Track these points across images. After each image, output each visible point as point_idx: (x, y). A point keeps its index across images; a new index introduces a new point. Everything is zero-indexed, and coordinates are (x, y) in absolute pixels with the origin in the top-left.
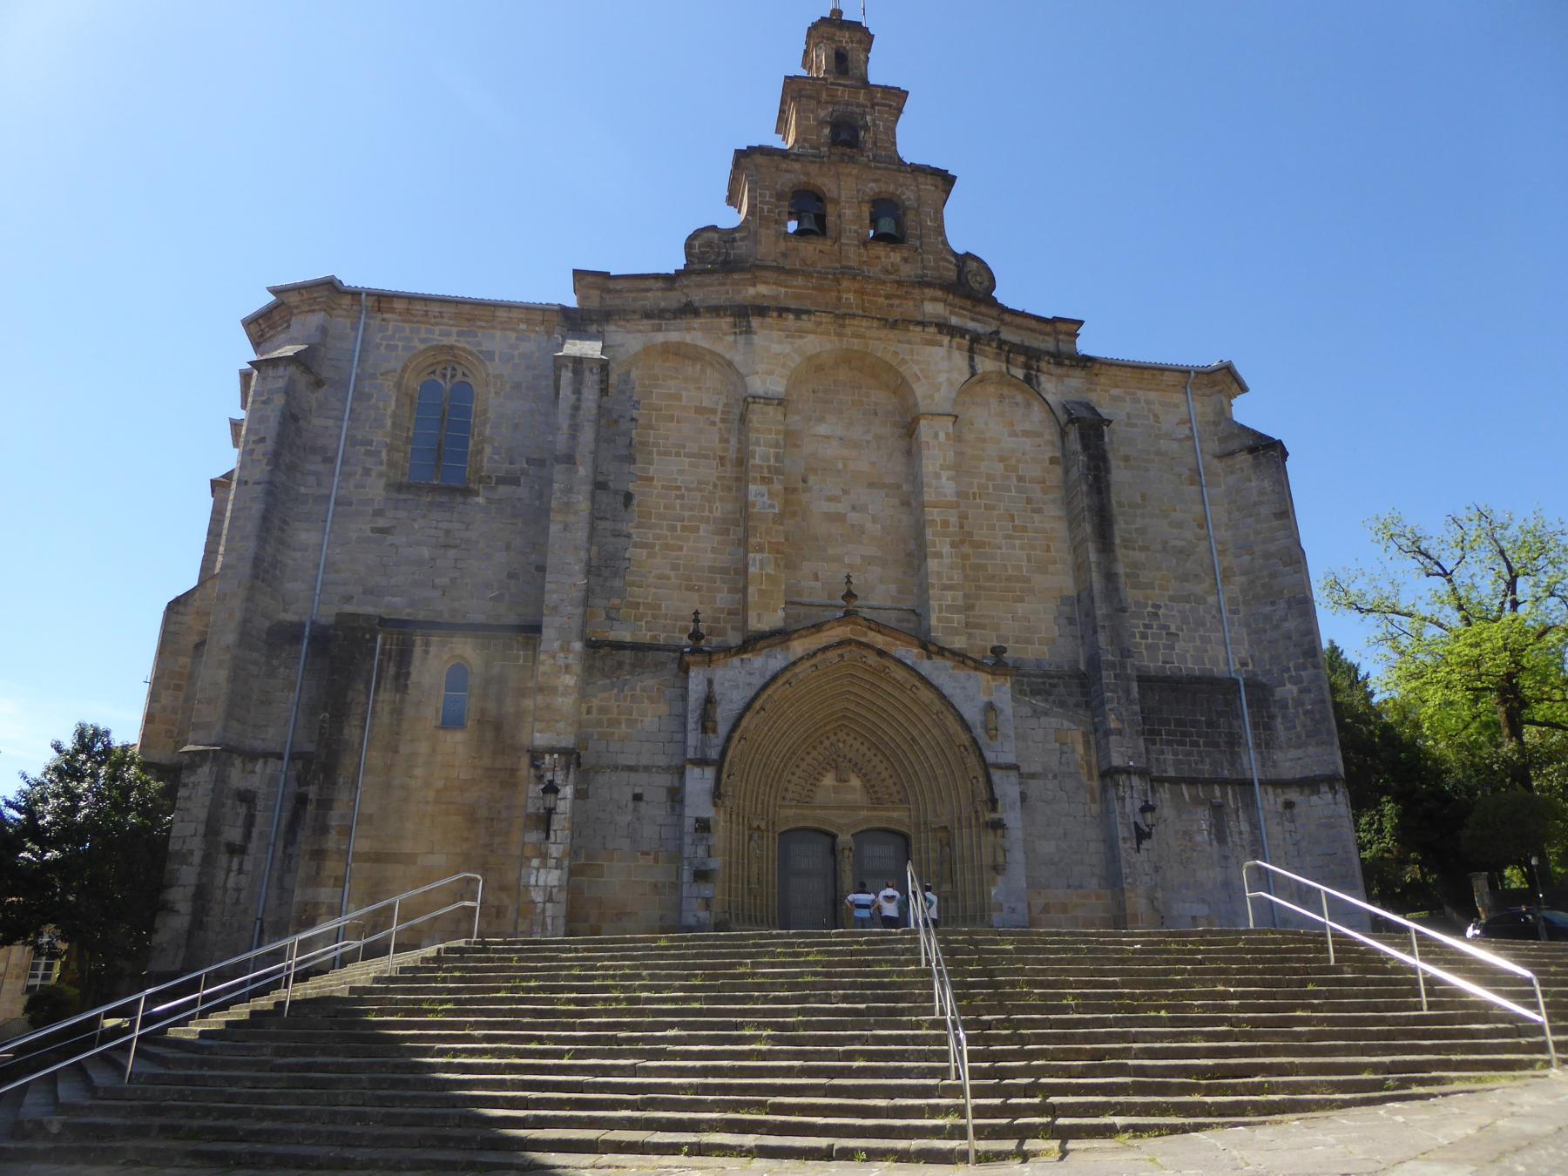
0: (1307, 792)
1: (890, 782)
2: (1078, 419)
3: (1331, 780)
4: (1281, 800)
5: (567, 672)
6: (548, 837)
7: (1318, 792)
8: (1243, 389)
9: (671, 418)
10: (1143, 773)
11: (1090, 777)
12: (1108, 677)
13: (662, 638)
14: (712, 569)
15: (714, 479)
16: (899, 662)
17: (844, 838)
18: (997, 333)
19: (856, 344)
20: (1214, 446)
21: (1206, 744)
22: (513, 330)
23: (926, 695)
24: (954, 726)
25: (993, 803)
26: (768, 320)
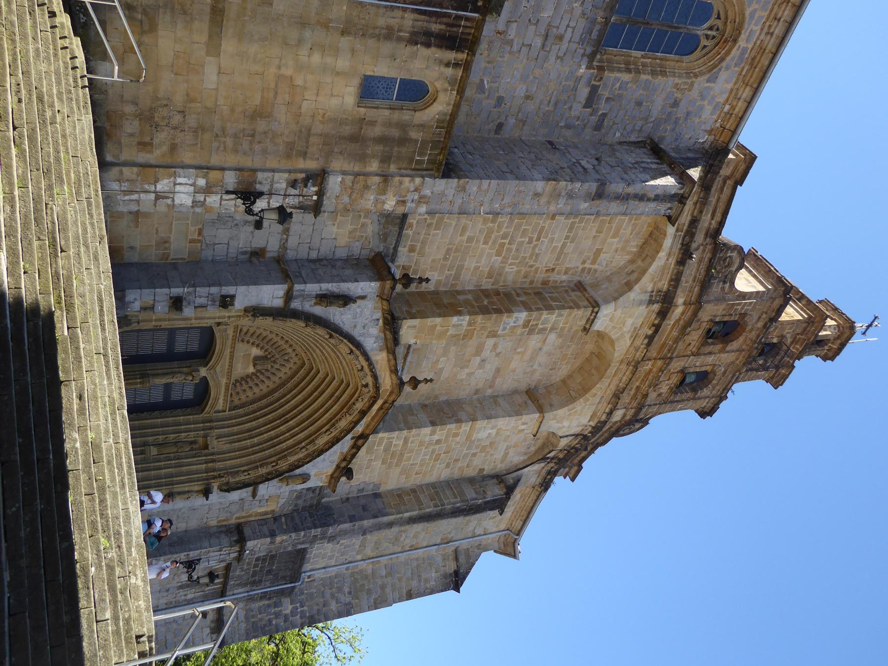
0: (213, 625)
5: (398, 202)
6: (228, 192)
7: (212, 633)
9: (599, 231)
11: (237, 518)
14: (461, 267)
15: (537, 265)
19: (612, 371)
21: (254, 571)
23: (322, 441)
25: (228, 488)
26: (654, 316)
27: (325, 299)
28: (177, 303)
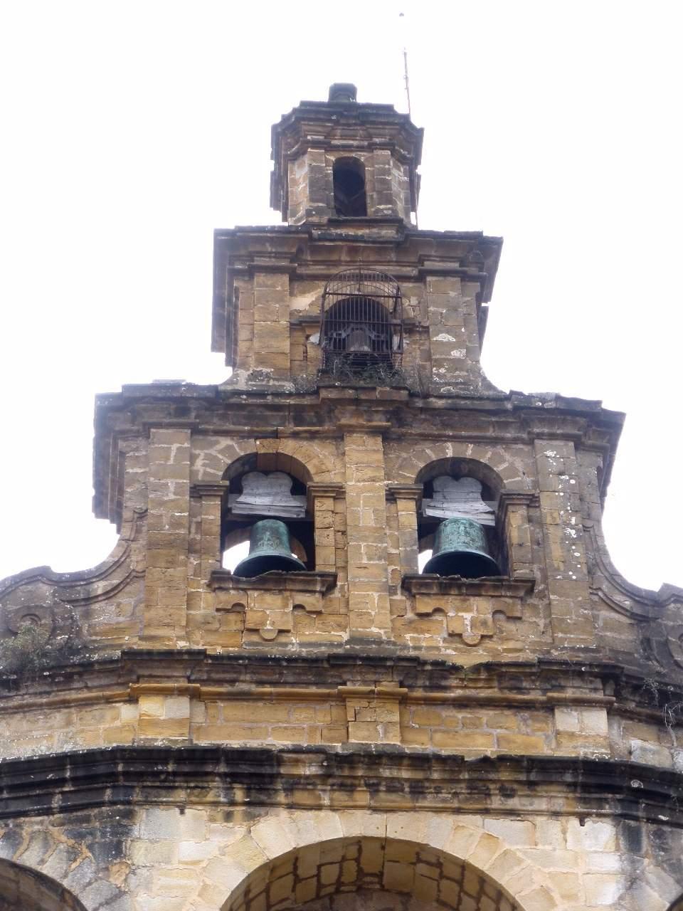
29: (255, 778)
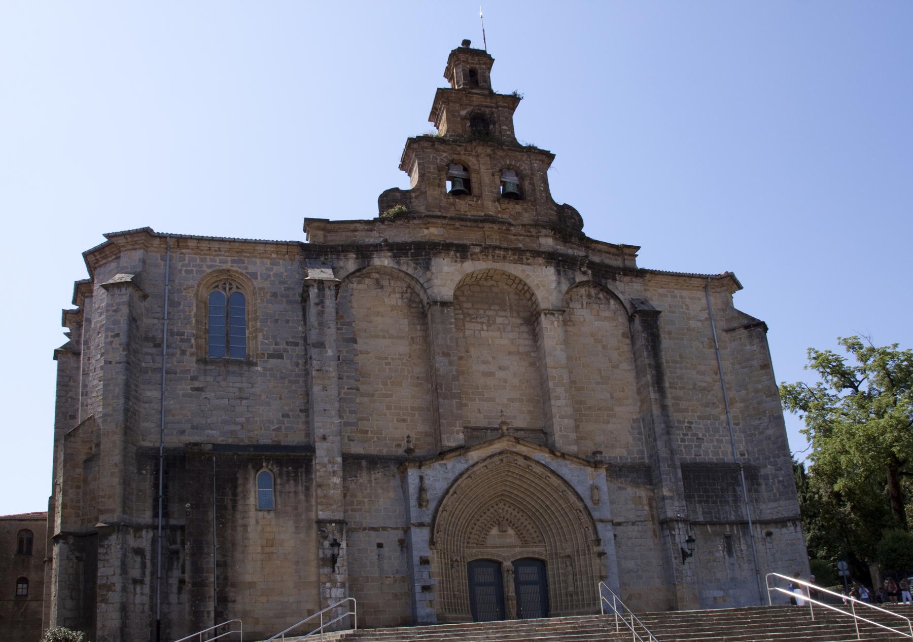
1: (532, 531)
2: (640, 311)
3: (793, 520)
4: (764, 531)
5: (334, 476)
6: (334, 571)
7: (786, 526)
8: (740, 287)
10: (685, 521)
12: (664, 467)
13: (385, 452)
14: (413, 408)
16: (538, 462)
17: (507, 564)
18: (587, 257)
20: (723, 324)
22: (268, 258)
23: (554, 481)
24: (573, 499)
25: (598, 542)
27: (421, 503)
28: (426, 588)
29: (462, 251)
